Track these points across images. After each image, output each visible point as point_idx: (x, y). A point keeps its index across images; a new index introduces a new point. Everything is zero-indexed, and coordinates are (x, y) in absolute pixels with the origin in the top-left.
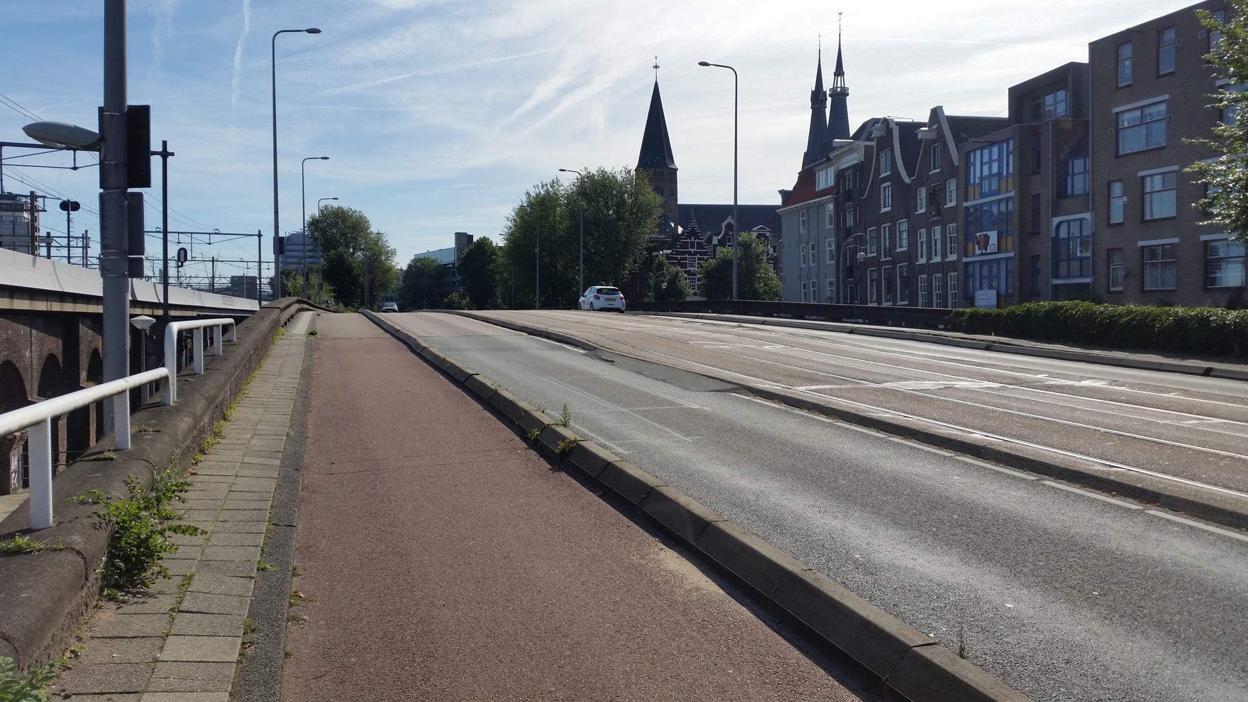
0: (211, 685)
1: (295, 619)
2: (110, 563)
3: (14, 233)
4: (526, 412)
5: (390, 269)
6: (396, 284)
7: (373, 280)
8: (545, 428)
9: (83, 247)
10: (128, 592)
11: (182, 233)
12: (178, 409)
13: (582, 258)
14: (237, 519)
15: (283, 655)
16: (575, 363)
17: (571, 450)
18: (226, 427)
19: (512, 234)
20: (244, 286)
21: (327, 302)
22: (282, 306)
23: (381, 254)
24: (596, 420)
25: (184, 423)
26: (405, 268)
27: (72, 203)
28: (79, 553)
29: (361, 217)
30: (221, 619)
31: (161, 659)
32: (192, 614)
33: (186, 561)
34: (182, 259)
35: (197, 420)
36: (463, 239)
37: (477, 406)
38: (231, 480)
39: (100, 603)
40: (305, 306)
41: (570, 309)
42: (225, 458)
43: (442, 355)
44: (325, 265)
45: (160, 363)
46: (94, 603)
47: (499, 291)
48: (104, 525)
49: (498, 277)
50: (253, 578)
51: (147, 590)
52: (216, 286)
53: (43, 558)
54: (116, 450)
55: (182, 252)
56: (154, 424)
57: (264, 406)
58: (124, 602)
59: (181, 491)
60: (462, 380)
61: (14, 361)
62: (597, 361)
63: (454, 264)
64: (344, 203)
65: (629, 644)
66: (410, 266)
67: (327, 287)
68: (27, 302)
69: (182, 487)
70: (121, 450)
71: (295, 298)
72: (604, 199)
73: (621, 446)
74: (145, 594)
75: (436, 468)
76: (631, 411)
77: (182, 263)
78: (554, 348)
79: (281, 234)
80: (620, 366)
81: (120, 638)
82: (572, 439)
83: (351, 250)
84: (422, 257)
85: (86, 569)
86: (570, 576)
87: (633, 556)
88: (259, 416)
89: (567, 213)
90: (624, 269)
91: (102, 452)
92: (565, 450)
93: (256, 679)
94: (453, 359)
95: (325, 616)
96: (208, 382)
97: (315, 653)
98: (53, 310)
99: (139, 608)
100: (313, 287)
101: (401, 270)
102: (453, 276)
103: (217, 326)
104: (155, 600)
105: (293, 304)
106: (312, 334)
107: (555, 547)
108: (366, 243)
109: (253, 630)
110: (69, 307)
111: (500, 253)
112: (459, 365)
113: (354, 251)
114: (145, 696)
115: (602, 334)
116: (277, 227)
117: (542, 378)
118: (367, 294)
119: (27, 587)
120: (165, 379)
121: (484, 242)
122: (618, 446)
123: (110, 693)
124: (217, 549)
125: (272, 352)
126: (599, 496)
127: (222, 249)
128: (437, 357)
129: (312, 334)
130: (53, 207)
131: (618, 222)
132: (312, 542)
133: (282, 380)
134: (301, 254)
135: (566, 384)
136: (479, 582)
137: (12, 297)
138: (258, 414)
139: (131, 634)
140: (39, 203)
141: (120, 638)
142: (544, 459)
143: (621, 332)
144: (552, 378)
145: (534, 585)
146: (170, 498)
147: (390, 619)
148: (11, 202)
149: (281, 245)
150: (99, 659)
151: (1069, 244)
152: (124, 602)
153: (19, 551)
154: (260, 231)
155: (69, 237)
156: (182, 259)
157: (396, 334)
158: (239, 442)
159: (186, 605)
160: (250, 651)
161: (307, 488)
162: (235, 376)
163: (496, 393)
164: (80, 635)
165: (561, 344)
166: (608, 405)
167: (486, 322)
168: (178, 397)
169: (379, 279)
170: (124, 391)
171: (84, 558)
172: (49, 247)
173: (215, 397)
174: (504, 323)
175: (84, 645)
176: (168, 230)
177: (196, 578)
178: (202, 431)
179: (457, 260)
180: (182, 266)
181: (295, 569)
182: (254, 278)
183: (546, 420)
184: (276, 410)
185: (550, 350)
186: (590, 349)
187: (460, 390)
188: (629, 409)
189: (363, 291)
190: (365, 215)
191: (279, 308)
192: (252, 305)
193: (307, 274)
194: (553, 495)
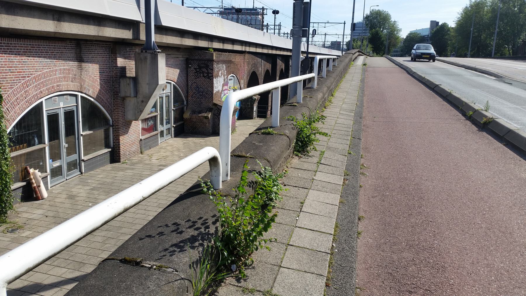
0: (333, 191)
1: (362, 174)
2: (296, 143)
3: (255, 24)
4: (466, 103)
5: (398, 38)
6: (400, 45)
7: (390, 43)
8: (475, 111)
9: (279, 29)
10: (302, 154)
11: (315, 23)
12: (317, 90)
13: (496, 33)
14: (339, 134)
15: (359, 187)
16: (490, 83)
17: (489, 122)
18: (333, 99)
19: (459, 21)
20: (335, 45)
22: (353, 53)
23: (395, 31)
24: (502, 110)
25: (320, 96)
26: (405, 37)
27: (276, 11)
28: (288, 137)
29: (387, 14)
30: (336, 169)
31: (315, 179)
32: (325, 165)
33: (321, 146)
34: (314, 34)
35: (324, 95)
36: (434, 24)
37: (440, 99)
38: (336, 119)
39: (293, 156)
40: (361, 54)
41: (487, 58)
42: (333, 111)
43: (423, 76)
44: (370, 36)
45: (311, 71)
46: (291, 156)
47: (449, 48)
48: (295, 129)
49: (449, 42)
50: (346, 156)
51: (308, 154)
52: (326, 45)
53: (277, 137)
54: (297, 103)
55: (314, 31)
56: (310, 95)
57: (347, 92)
58: (301, 157)
59: (322, 119)
60: (433, 88)
61: (256, 71)
62: (502, 83)
63: (428, 36)
64: (381, 8)
65: (520, 212)
66: (407, 37)
67: (370, 46)
69: (323, 117)
70: (299, 103)
71: (358, 50)
72: (513, 2)
73: (516, 124)
74: (308, 156)
75: (421, 124)
76: (522, 108)
77: (314, 35)
78: (479, 76)
79: (355, 22)
80: (515, 86)
81: (300, 169)
82: (491, 117)
83: (382, 29)
84: (413, 32)
85: (290, 143)
86: (488, 177)
87: (522, 174)
88: (345, 96)
89: (491, 10)
90: (519, 39)
91: (293, 103)
92: (486, 122)
93: (349, 192)
94: (428, 77)
95: (375, 175)
96: (328, 81)
97: (371, 188)
98: (269, 53)
99: (306, 160)
100: (364, 46)
101: (403, 38)
102: (427, 41)
103: (331, 59)
104: (312, 158)
105: (356, 52)
106: (365, 65)
107: (480, 164)
108: (389, 26)
109: (348, 175)
110: (274, 52)
111: (452, 31)
112: (432, 80)
113: (383, 30)
114: (310, 190)
115: (506, 70)
116: (353, 19)
117: (473, 89)
118: (387, 49)
119: (273, 146)
120: (314, 78)
121: (444, 25)
122: (514, 123)
123: (299, 187)
124: (332, 143)
125: (349, 72)
126: (504, 145)
127: (330, 30)
128: (421, 76)
129: (365, 65)
130: (270, 13)
131: (520, 14)
132: (368, 146)
133: (353, 82)
134: (361, 32)
135: (485, 93)
136: (443, 173)
138: (344, 95)
139: (304, 169)
140: (265, 11)
141: (300, 169)
142: (474, 125)
143: (516, 70)
144: (478, 89)
145: (469, 179)
146: (319, 121)
147: (403, 181)
148: (255, 12)
149: (354, 26)
150: (294, 175)
152: (301, 157)
153: (269, 134)
154: (345, 21)
155: (275, 25)
156: (314, 34)
157: (401, 66)
158: (338, 105)
159: (322, 162)
160: (347, 182)
161: (365, 126)
162: (336, 80)
163: (450, 93)
164: (288, 166)
165: (483, 74)
166: (508, 104)
167: (444, 62)
168: (317, 86)
169: (393, 42)
170: (301, 81)
171: (290, 139)
172: (267, 29)
173: (330, 87)
174: (453, 63)
175: (289, 169)
176: (310, 22)
177: (326, 152)
178: (325, 100)
179: (430, 34)
180: (314, 37)
181: (362, 155)
182: (340, 42)
183: (476, 107)
184: (352, 94)
185: (476, 77)
186: (498, 77)
187: (432, 91)
188: (521, 107)
189: (385, 48)
190: (390, 13)
191: (352, 53)
192: (339, 53)
194: (479, 142)
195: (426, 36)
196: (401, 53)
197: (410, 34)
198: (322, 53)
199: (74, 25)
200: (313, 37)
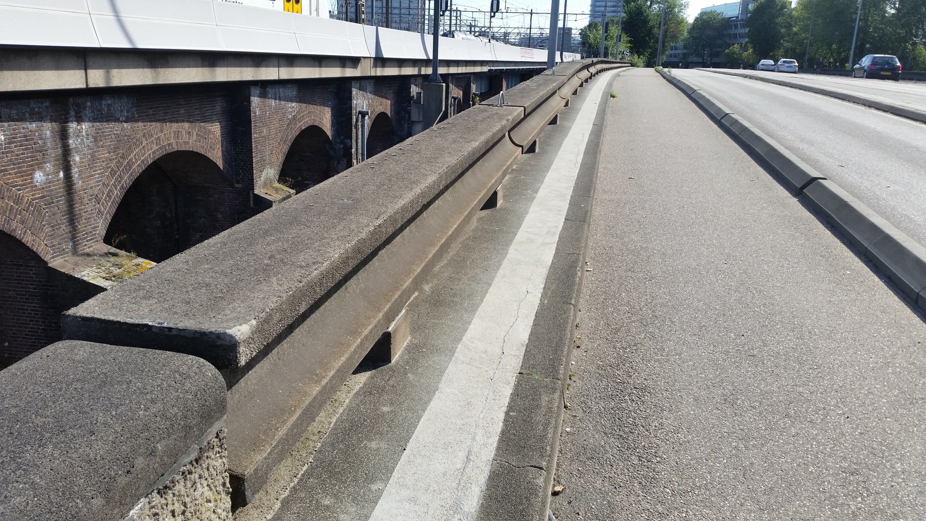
21: (623, 53)
23: (675, 6)
34: (495, 10)
63: (737, 17)
66: (696, 19)
67: (625, 38)
68: (411, 69)
77: (495, 13)
100: (612, 38)
113: (651, 4)
137: (107, 68)
151: (602, 2)
156: (495, 10)
169: (671, 30)
180: (494, 16)
189: (657, 41)
193: (607, 24)
195: (734, 17)
196: (685, 51)
197: (703, 14)
198: (143, 43)
199: (231, 69)
200: (491, 17)
